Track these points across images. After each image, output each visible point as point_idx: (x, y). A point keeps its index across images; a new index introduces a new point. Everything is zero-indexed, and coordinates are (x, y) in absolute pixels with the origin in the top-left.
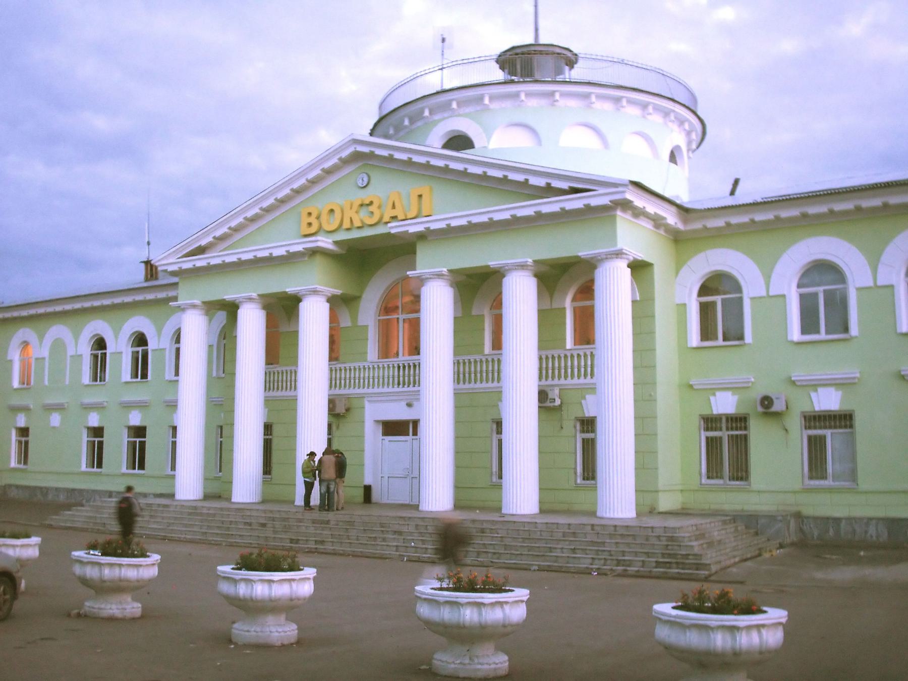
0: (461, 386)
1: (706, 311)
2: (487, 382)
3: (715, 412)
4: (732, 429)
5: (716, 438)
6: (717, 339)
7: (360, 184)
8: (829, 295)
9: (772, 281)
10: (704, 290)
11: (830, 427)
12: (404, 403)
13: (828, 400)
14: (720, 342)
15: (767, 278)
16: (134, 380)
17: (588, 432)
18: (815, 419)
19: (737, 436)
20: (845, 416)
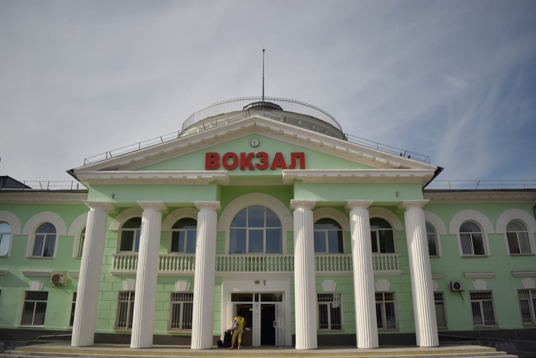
0: (320, 272)
1: (38, 239)
2: (326, 270)
3: (525, 288)
4: (474, 299)
5: (324, 305)
6: (40, 255)
7: (253, 144)
8: (48, 236)
9: (493, 229)
10: (462, 229)
11: (481, 299)
12: (253, 282)
13: (481, 286)
14: (473, 254)
15: (495, 228)
16: (174, 254)
17: (389, 300)
18: (474, 295)
19: (486, 302)
20: (329, 294)
